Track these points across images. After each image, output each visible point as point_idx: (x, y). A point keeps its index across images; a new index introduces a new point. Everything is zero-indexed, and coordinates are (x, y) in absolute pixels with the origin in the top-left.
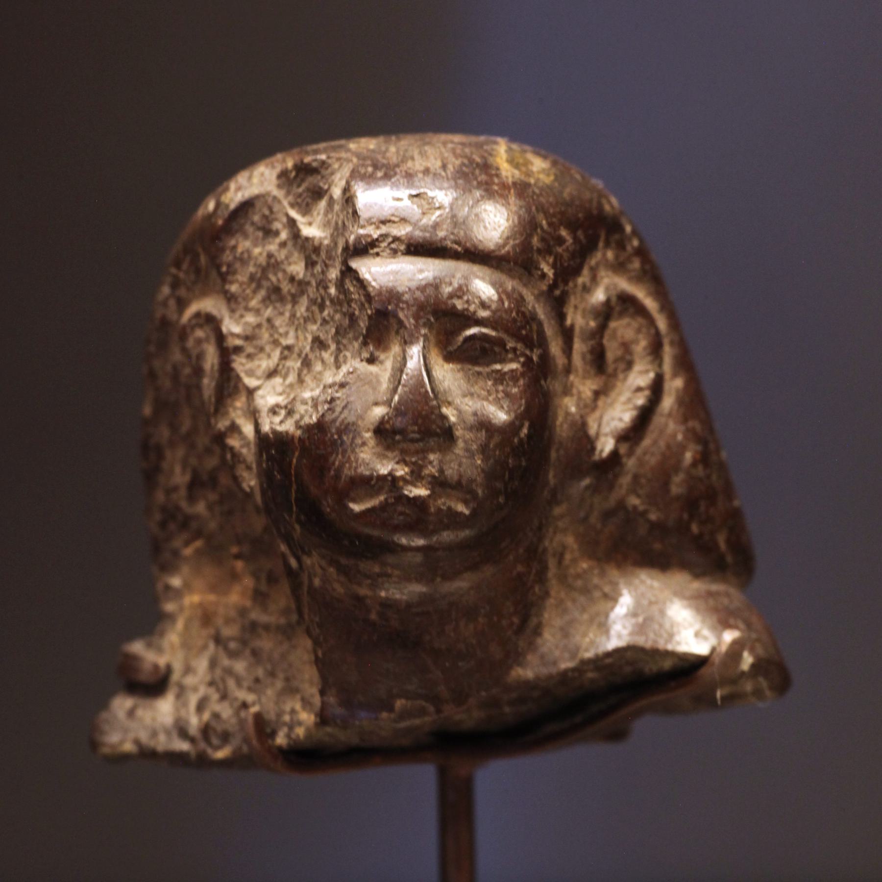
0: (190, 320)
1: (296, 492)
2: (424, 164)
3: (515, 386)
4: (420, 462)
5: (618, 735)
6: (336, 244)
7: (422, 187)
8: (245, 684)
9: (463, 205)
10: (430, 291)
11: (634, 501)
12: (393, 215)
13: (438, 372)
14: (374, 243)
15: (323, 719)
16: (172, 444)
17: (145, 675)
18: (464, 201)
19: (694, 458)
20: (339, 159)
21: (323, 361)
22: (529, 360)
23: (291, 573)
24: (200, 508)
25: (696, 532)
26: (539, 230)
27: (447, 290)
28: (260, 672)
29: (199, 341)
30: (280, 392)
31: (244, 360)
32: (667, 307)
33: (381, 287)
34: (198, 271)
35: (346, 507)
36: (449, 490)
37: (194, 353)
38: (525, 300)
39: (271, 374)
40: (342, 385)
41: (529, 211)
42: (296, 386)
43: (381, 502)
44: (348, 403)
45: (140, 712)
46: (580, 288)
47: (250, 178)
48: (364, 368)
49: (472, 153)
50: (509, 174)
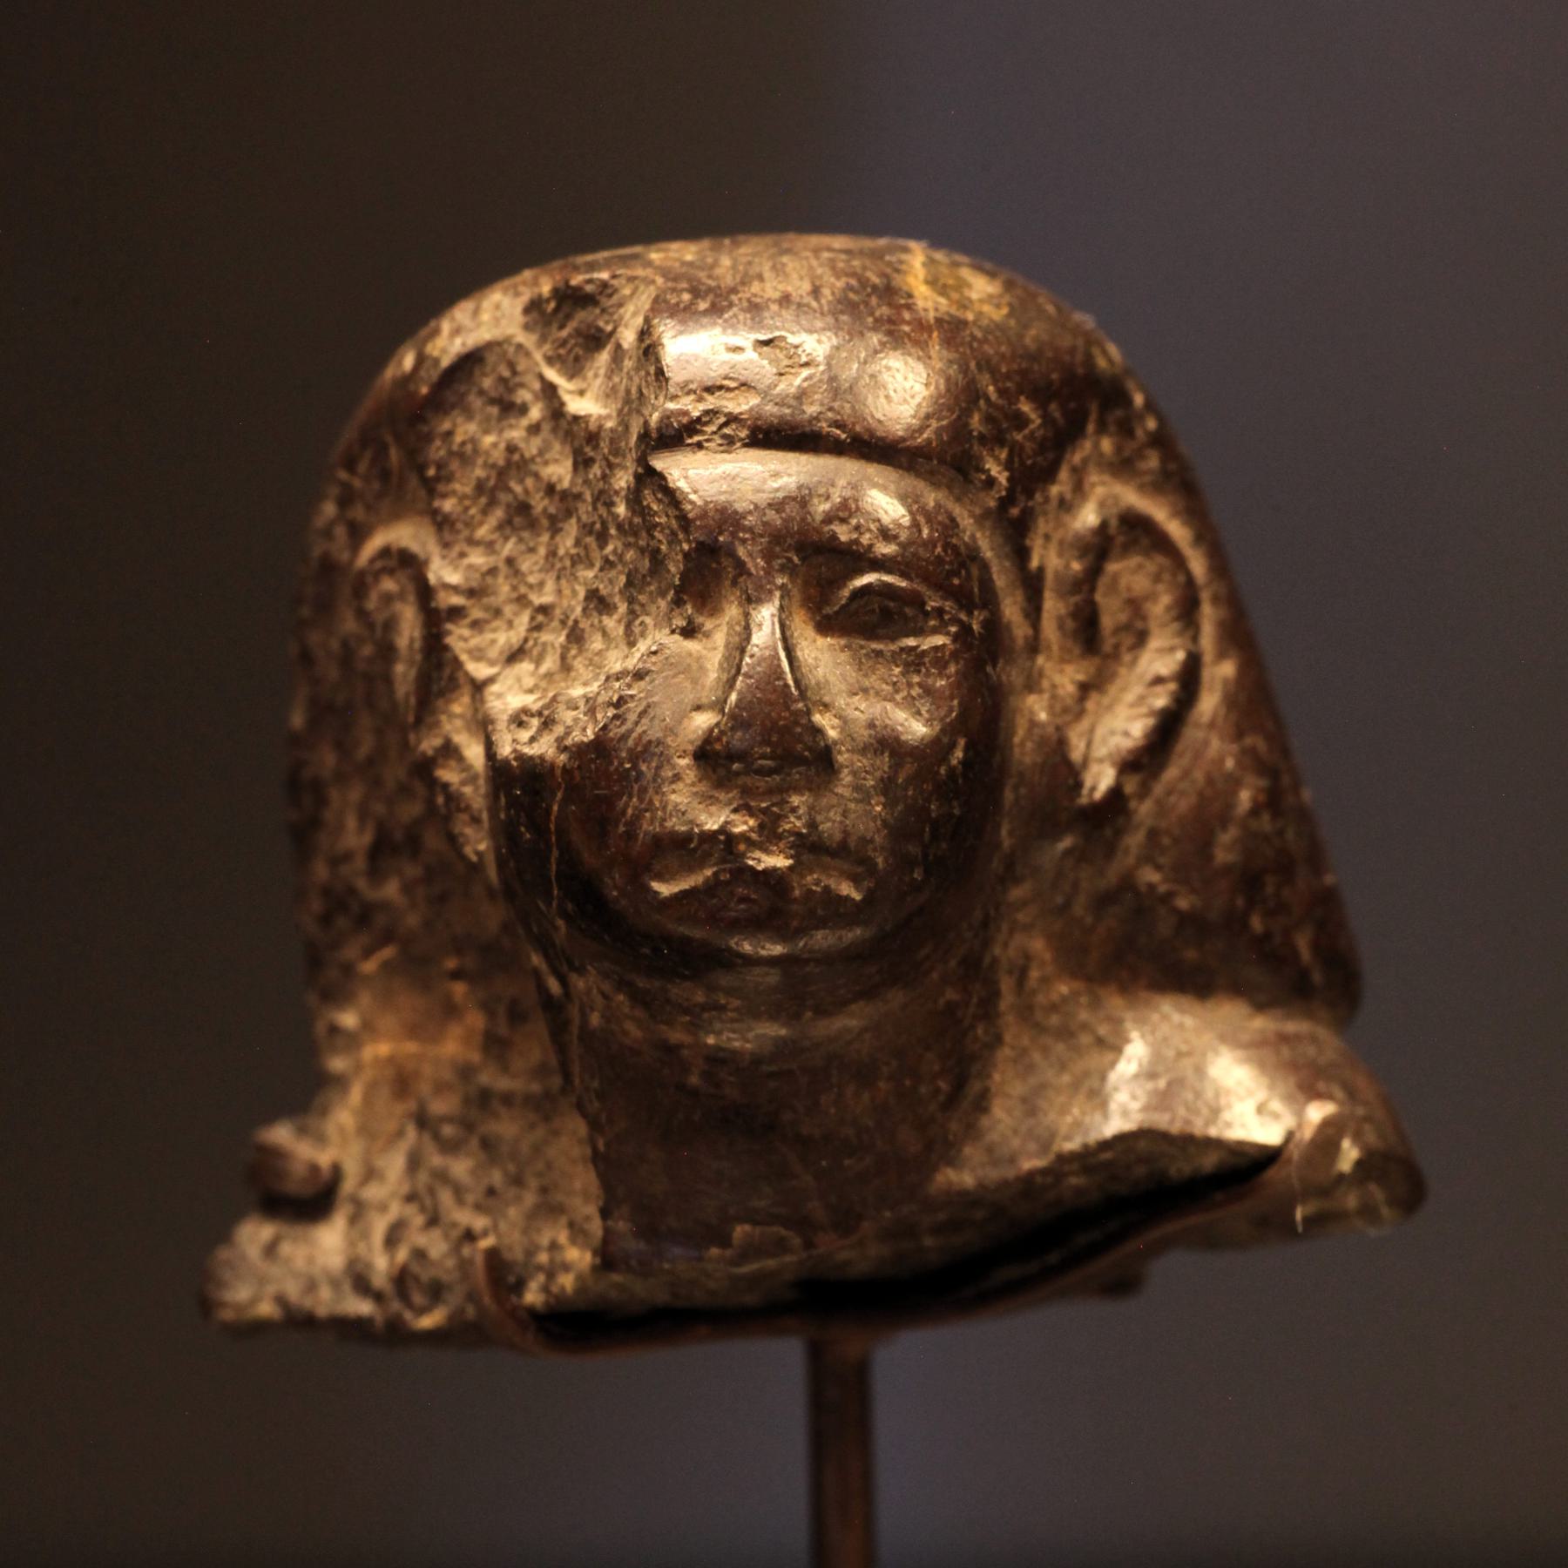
0: (372, 561)
2: (781, 287)
3: (940, 675)
5: (1123, 1285)
6: (627, 428)
7: (777, 328)
10: (791, 510)
11: (1150, 876)
12: (726, 378)
14: (693, 426)
15: (607, 1259)
17: (295, 1183)
20: (631, 279)
21: (605, 634)
22: (966, 629)
24: (391, 890)
25: (1256, 931)
26: (982, 402)
27: (821, 508)
28: (496, 1177)
29: (388, 599)
31: (466, 632)
32: (1207, 536)
33: (707, 503)
34: (385, 475)
35: (649, 889)
36: (827, 859)
37: (379, 618)
38: (957, 526)
39: (514, 656)
40: (639, 675)
41: (965, 370)
42: (557, 677)
43: (707, 879)
44: (649, 706)
45: (286, 1248)
46: (1054, 503)
47: (476, 312)
48: (678, 645)
49: (865, 268)
50: (930, 305)
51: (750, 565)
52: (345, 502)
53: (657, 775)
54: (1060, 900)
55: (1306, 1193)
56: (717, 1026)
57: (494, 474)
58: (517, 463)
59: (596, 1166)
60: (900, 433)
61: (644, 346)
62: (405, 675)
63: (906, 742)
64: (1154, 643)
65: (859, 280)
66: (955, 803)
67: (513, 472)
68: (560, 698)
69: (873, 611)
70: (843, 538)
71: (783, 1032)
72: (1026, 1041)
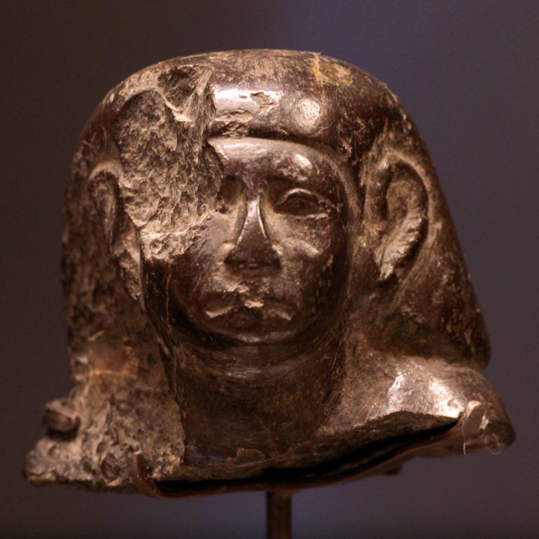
0: (96, 177)
1: (169, 303)
2: (262, 72)
3: (324, 230)
4: (257, 283)
5: (394, 471)
6: (199, 127)
7: (260, 89)
8: (131, 434)
9: (288, 102)
11: (407, 309)
12: (239, 108)
13: (270, 220)
14: (226, 128)
15: (186, 461)
16: (82, 263)
17: (61, 427)
18: (289, 99)
19: (449, 278)
20: (202, 67)
21: (189, 210)
22: (334, 211)
23: (164, 358)
24: (102, 308)
25: (450, 332)
26: (342, 119)
27: (277, 162)
28: (142, 426)
29: (102, 192)
30: (159, 230)
31: (134, 207)
32: (431, 172)
33: (231, 159)
34: (102, 143)
35: (205, 315)
36: (277, 304)
37: (99, 200)
38: (331, 169)
39: (153, 217)
40: (203, 228)
41: (335, 106)
42: (170, 227)
43: (229, 311)
44: (206, 241)
45: (57, 451)
46: (370, 159)
47: (139, 78)
49: (295, 64)
50: (321, 80)
51: (248, 185)
52: (86, 152)
53: (209, 268)
54: (370, 319)
55: (467, 437)
56: (232, 368)
57: (145, 144)
58: (155, 139)
59: (182, 423)
60: (309, 132)
61: (207, 95)
62: (109, 224)
63: (309, 257)
64: (409, 215)
65: (293, 70)
66: (329, 281)
67: (153, 143)
68: (171, 236)
69: (297, 204)
70: (285, 174)
71: (258, 372)
72: (356, 375)
